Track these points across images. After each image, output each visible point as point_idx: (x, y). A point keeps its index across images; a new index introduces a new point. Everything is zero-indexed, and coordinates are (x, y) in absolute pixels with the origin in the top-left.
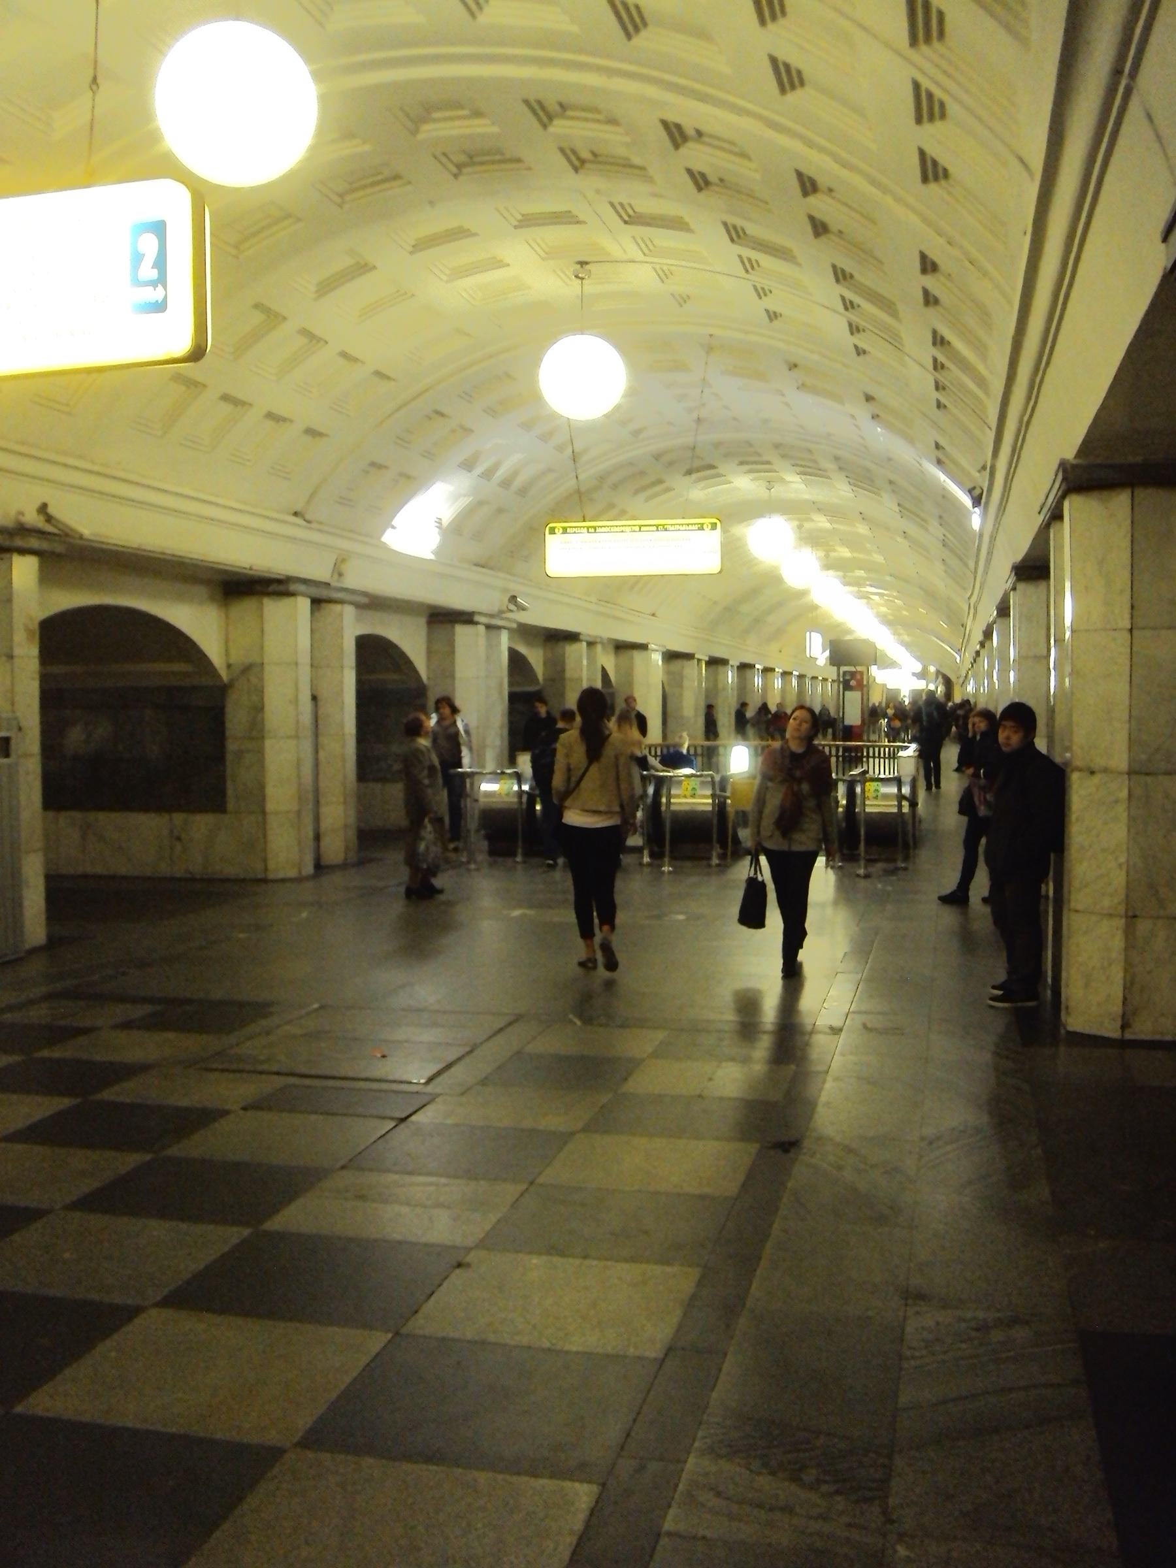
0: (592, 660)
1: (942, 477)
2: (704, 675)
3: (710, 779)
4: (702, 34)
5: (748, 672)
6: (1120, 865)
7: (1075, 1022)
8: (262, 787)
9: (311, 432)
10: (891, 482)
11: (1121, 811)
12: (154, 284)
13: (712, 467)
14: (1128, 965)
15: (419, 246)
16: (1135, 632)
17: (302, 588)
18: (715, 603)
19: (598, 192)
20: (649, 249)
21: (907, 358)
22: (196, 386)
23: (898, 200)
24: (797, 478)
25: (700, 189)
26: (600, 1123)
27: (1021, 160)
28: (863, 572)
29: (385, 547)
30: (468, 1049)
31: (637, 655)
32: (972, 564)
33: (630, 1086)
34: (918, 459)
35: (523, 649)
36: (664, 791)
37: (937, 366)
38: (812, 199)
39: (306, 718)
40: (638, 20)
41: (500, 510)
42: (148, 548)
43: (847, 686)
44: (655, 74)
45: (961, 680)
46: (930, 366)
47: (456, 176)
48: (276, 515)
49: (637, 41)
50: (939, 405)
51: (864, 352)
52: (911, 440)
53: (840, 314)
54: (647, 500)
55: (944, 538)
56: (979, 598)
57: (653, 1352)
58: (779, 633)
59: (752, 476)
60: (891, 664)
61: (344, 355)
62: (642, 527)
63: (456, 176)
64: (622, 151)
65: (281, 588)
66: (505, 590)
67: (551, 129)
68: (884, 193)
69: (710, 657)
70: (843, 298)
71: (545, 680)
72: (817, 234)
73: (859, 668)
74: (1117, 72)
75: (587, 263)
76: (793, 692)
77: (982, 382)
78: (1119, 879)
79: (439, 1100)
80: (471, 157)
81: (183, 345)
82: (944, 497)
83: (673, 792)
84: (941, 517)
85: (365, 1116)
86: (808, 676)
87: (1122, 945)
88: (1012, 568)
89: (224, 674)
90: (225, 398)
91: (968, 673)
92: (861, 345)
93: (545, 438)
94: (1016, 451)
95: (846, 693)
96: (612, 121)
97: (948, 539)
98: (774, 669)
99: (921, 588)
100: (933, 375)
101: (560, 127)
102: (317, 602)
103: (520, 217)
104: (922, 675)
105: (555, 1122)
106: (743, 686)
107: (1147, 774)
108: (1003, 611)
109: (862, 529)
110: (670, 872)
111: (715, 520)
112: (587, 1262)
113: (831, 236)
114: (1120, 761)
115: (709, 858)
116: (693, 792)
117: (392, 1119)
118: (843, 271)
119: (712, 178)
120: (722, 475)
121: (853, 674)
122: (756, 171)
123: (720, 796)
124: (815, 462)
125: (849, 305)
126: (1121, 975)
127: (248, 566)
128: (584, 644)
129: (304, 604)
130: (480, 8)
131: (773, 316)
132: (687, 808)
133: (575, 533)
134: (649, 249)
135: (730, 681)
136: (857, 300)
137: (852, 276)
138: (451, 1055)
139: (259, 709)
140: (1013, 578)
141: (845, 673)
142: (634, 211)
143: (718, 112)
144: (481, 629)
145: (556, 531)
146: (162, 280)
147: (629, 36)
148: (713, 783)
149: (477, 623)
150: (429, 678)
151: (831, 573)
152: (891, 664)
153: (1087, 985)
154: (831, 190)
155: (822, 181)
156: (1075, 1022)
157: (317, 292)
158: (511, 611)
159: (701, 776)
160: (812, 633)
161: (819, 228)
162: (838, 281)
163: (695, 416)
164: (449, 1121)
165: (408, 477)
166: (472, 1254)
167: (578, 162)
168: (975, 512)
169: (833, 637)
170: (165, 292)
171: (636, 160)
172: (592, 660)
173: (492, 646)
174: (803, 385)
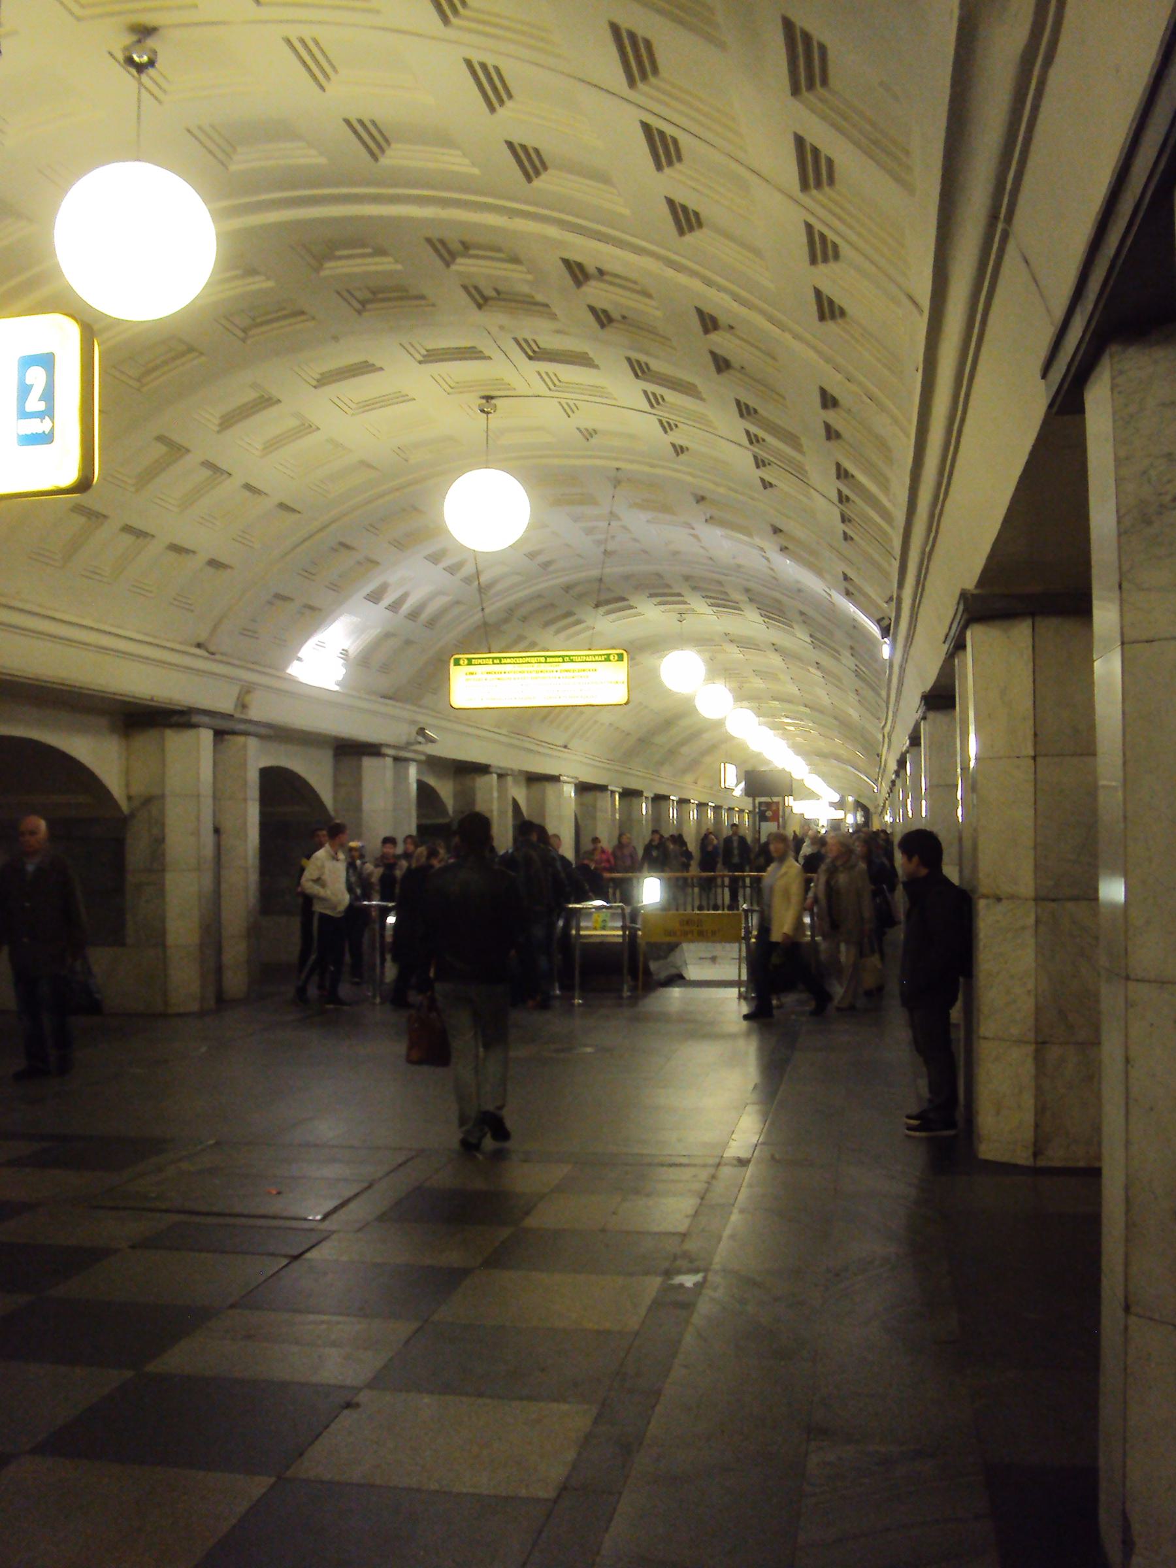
0: (502, 789)
1: (852, 609)
2: (617, 807)
3: (619, 911)
4: (603, 178)
5: (663, 804)
6: (1029, 992)
7: (988, 1150)
8: (163, 919)
9: (213, 563)
10: (802, 613)
11: (1029, 939)
12: (40, 415)
13: (623, 599)
14: (1039, 1091)
15: (323, 381)
16: (1039, 759)
17: (205, 719)
18: (628, 734)
19: (502, 328)
20: (555, 385)
21: (812, 490)
22: (97, 517)
23: (796, 336)
24: (709, 610)
25: (603, 326)
26: (497, 1259)
27: (911, 298)
28: (777, 703)
29: (292, 680)
30: (365, 1185)
31: (550, 788)
32: (884, 693)
33: (531, 1222)
34: (827, 590)
35: (432, 781)
36: (574, 923)
37: (843, 499)
38: (714, 337)
39: (208, 851)
40: (537, 163)
41: (408, 642)
42: (45, 678)
43: (763, 817)
44: (555, 214)
45: (880, 809)
46: (835, 499)
47: (359, 312)
48: (178, 647)
49: (536, 183)
50: (846, 537)
51: (771, 485)
52: (819, 572)
53: (746, 448)
54: (558, 632)
55: (856, 668)
56: (893, 727)
57: (546, 1493)
58: (693, 765)
59: (663, 607)
60: (811, 795)
61: (248, 487)
62: (548, 659)
63: (359, 312)
64: (525, 289)
65: (183, 720)
66: (414, 722)
67: (454, 267)
68: (783, 331)
69: (624, 789)
70: (748, 432)
71: (454, 812)
72: (719, 370)
73: (775, 799)
74: (993, 217)
75: (492, 398)
76: (709, 823)
77: (886, 515)
78: (1027, 1005)
79: (335, 1236)
80: (374, 293)
81: (69, 475)
82: (854, 627)
83: (583, 924)
84: (852, 648)
85: (254, 1254)
86: (724, 807)
87: (1033, 1071)
88: (922, 699)
89: (125, 806)
90: (128, 529)
91: (885, 802)
92: (767, 478)
93: (452, 570)
94: (920, 583)
95: (762, 823)
96: (515, 260)
97: (860, 669)
98: (690, 800)
99: (836, 718)
100: (838, 507)
101: (463, 265)
102: (220, 735)
103: (425, 353)
104: (840, 805)
105: (453, 1258)
106: (658, 817)
107: (1053, 900)
108: (915, 741)
109: (776, 660)
110: (579, 1005)
111: (621, 651)
112: (481, 1401)
113: (732, 371)
114: (1026, 885)
115: (621, 990)
116: (603, 924)
117: (286, 1256)
118: (747, 406)
119: (615, 315)
120: (631, 607)
121: (768, 805)
122: (657, 309)
123: (630, 929)
124: (726, 593)
125: (753, 439)
126: (1032, 1101)
127: (149, 698)
128: (495, 776)
129: (206, 736)
130: (382, 151)
131: (679, 450)
132: (598, 940)
133: (480, 664)
134: (555, 385)
135: (644, 813)
136: (761, 434)
137: (756, 411)
138: (348, 1193)
139: (160, 840)
140: (923, 708)
141: (760, 803)
142: (539, 347)
143: (617, 252)
144: (389, 761)
145: (461, 662)
146: (49, 412)
147: (529, 179)
148: (623, 916)
149: (384, 755)
150: (336, 811)
151: (745, 704)
152: (811, 795)
153: (998, 1113)
154: (731, 327)
155: (723, 319)
156: (988, 1150)
157: (221, 425)
158: (420, 743)
159: (610, 908)
160: (727, 764)
161: (722, 364)
162: (742, 415)
163: (602, 549)
164: (345, 1258)
165: (312, 608)
166: (362, 1394)
167: (482, 299)
168: (885, 642)
169: (749, 768)
170: (51, 424)
171: (540, 298)
172: (502, 789)
173: (400, 778)
174: (711, 518)
